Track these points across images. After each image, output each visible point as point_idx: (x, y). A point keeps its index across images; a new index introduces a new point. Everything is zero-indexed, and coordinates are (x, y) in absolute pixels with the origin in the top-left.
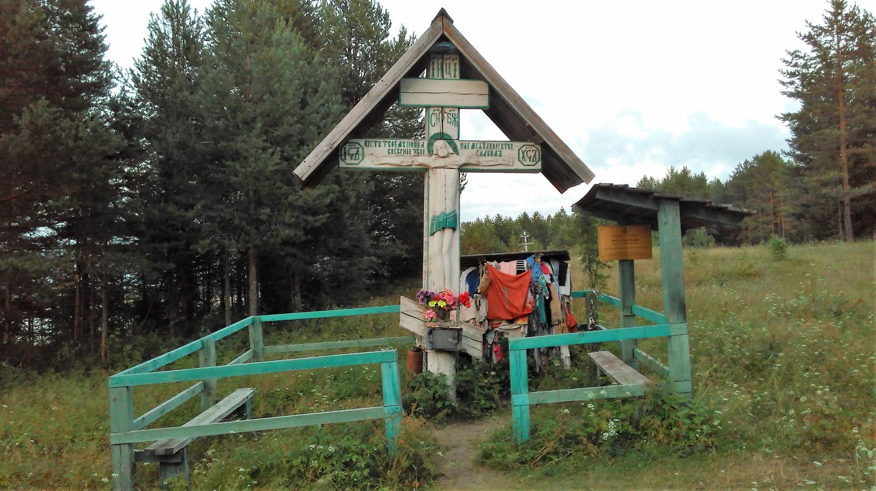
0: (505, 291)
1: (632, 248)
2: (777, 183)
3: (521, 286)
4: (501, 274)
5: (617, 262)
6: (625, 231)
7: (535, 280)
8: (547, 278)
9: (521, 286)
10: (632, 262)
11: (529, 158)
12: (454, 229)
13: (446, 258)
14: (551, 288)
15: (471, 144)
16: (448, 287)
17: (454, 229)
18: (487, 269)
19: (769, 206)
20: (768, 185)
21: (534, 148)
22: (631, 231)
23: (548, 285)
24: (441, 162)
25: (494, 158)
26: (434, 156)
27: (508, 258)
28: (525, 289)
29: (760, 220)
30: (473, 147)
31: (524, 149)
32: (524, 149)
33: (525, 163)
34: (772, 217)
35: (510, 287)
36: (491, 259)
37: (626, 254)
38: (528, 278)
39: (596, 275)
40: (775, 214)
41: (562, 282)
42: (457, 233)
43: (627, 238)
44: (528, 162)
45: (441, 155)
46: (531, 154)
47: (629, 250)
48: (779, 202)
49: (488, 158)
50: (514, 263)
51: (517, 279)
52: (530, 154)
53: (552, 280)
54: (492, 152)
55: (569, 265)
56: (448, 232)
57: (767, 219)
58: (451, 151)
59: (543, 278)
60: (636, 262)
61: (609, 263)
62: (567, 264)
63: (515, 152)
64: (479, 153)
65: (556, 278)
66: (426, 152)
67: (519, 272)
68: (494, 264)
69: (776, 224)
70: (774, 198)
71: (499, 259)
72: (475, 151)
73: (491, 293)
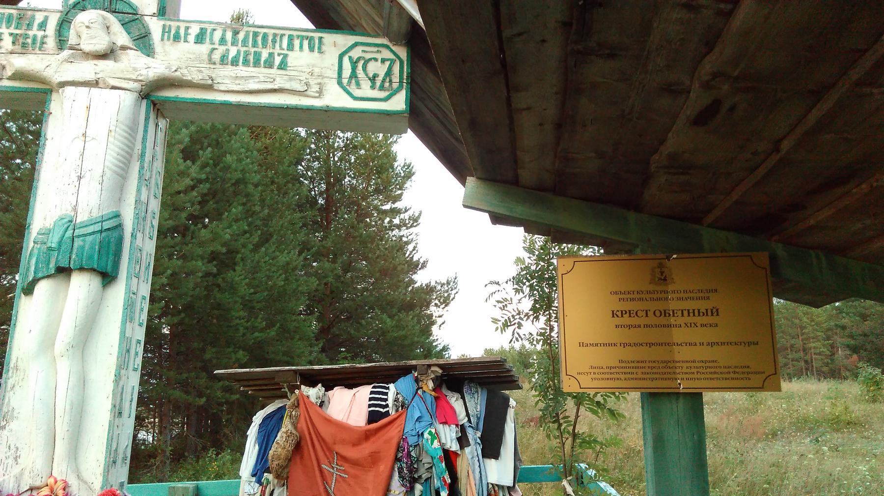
0: (333, 470)
1: (692, 345)
2: (805, 319)
3: (374, 458)
4: (329, 421)
5: (635, 396)
6: (662, 278)
7: (412, 440)
8: (449, 436)
9: (374, 458)
10: (695, 399)
11: (373, 79)
12: (107, 277)
13: (65, 367)
14: (462, 466)
15: (195, 30)
16: (61, 470)
17: (107, 277)
18: (296, 406)
19: (798, 343)
20: (797, 321)
21: (386, 54)
22: (685, 274)
23: (449, 458)
24: (87, 70)
25: (262, 71)
26: (66, 53)
27: (350, 380)
28: (383, 468)
29: (790, 356)
30: (200, 38)
31: (356, 53)
32: (356, 53)
33: (357, 93)
34: (801, 354)
35: (344, 459)
36: (311, 379)
37: (668, 367)
38: (393, 433)
39: (575, 436)
40: (804, 350)
41: (491, 449)
42: (118, 293)
43: (673, 305)
44: (366, 90)
45: (87, 47)
46: (378, 68)
47: (682, 354)
48: (808, 339)
49: (242, 70)
50: (364, 392)
51: (367, 435)
52: (373, 68)
53: (463, 441)
54: (257, 55)
55: (512, 403)
56: (82, 285)
57: (797, 356)
58: (122, 38)
59: (436, 436)
60: (707, 396)
61: (611, 403)
62: (506, 400)
63: (330, 59)
64: (217, 56)
65: (474, 436)
66: (51, 43)
67: (373, 417)
68: (313, 393)
69: (806, 362)
70: (803, 334)
71: (330, 381)
72: (204, 48)
73: (297, 472)
